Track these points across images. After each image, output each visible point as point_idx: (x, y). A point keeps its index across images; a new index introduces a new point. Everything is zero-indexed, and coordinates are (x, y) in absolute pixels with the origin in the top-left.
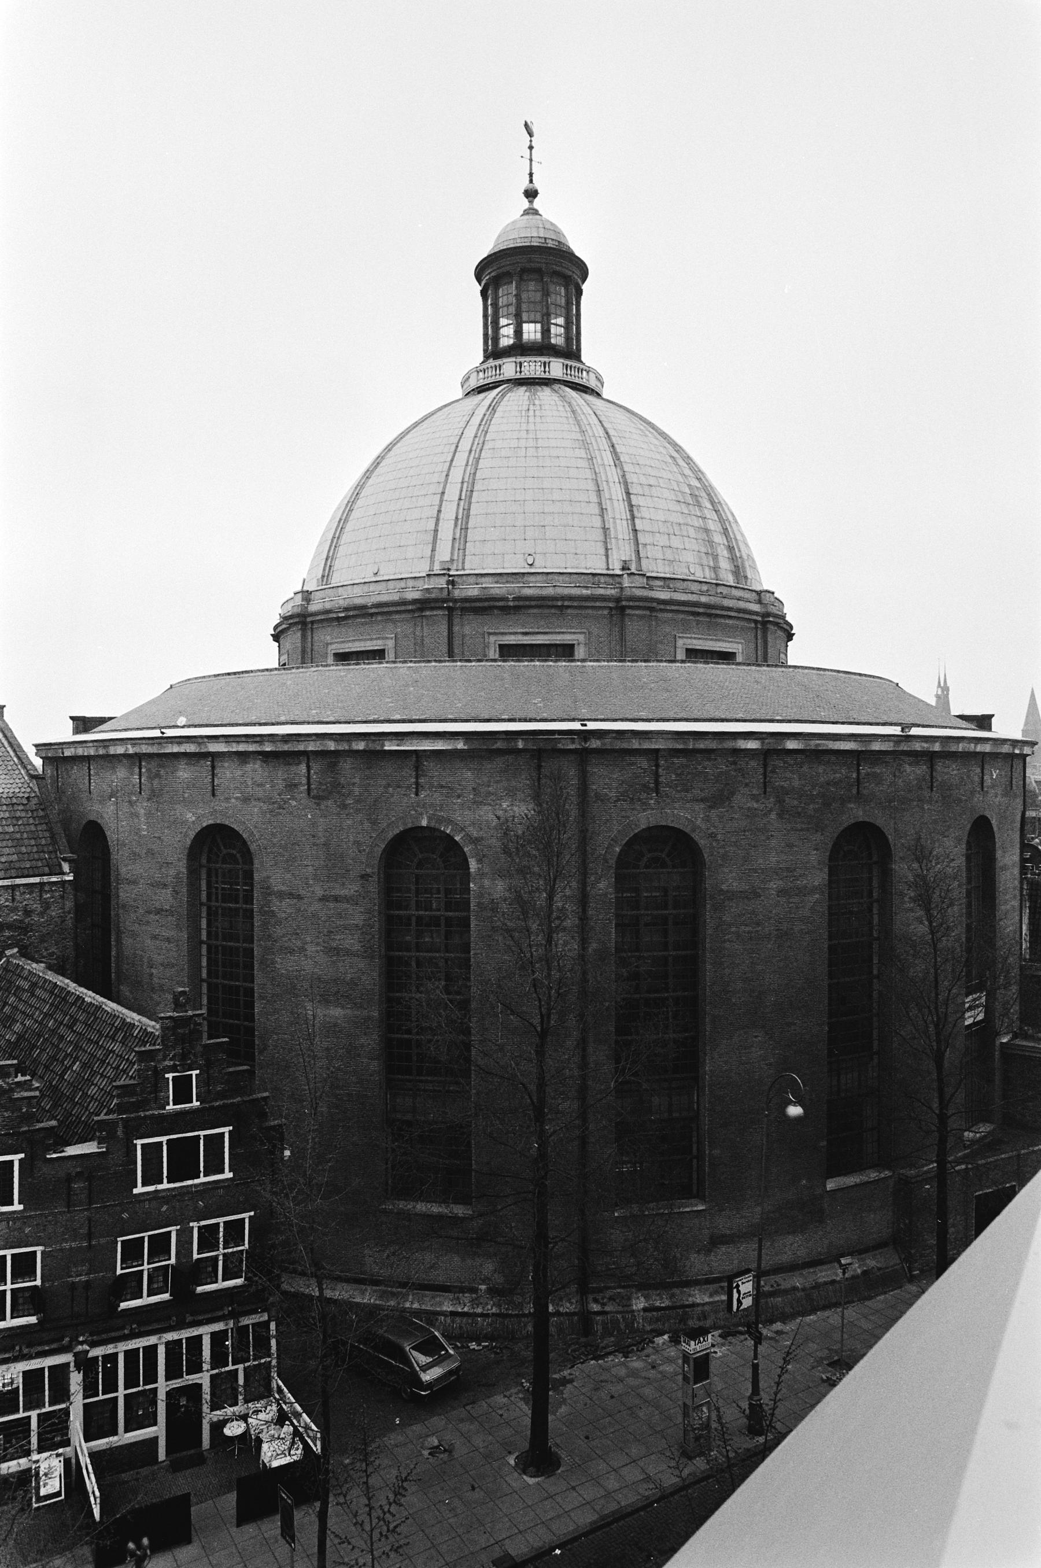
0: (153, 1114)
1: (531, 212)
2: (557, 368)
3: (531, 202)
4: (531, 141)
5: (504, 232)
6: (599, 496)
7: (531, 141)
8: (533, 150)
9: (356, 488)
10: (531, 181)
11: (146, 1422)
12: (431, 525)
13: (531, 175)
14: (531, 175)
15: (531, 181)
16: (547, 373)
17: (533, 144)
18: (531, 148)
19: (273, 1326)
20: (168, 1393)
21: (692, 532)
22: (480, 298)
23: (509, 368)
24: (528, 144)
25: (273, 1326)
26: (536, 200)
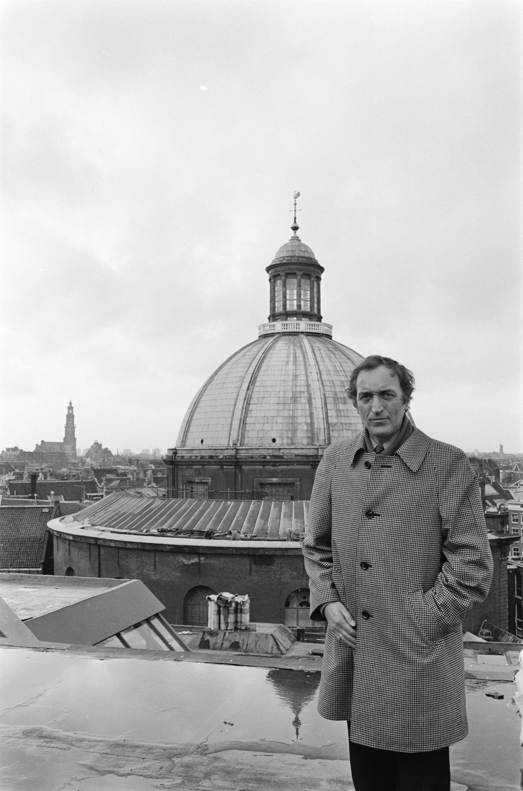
0: (515, 617)
1: (296, 239)
2: (304, 325)
3: (295, 232)
4: (295, 201)
5: (279, 252)
6: (308, 388)
7: (295, 201)
8: (297, 205)
9: (199, 395)
10: (295, 222)
11: (27, 454)
12: (233, 402)
13: (295, 218)
14: (295, 218)
15: (295, 222)
16: (298, 329)
17: (297, 203)
18: (295, 204)
19: (227, 595)
20: (65, 500)
21: (280, 420)
22: (268, 284)
23: (278, 326)
24: (294, 202)
25: (227, 595)
26: (298, 231)
